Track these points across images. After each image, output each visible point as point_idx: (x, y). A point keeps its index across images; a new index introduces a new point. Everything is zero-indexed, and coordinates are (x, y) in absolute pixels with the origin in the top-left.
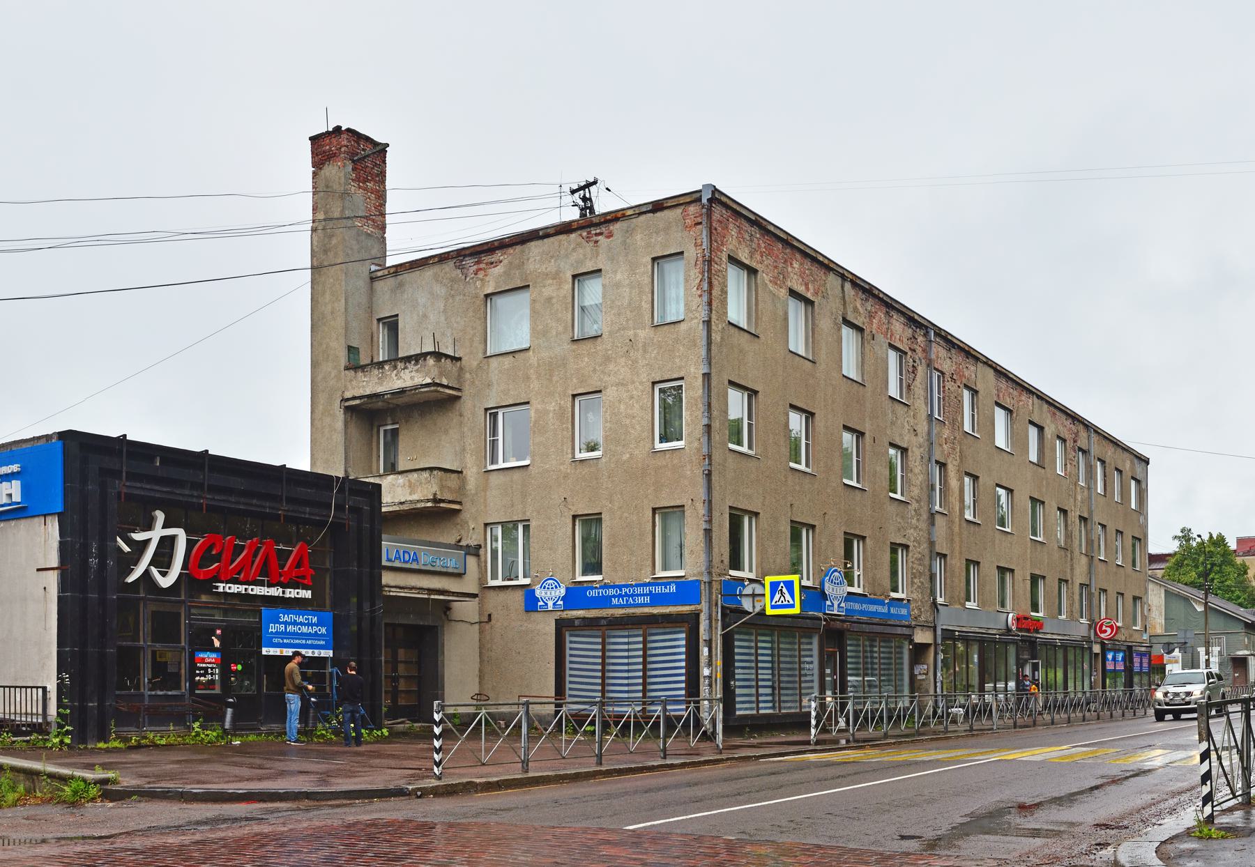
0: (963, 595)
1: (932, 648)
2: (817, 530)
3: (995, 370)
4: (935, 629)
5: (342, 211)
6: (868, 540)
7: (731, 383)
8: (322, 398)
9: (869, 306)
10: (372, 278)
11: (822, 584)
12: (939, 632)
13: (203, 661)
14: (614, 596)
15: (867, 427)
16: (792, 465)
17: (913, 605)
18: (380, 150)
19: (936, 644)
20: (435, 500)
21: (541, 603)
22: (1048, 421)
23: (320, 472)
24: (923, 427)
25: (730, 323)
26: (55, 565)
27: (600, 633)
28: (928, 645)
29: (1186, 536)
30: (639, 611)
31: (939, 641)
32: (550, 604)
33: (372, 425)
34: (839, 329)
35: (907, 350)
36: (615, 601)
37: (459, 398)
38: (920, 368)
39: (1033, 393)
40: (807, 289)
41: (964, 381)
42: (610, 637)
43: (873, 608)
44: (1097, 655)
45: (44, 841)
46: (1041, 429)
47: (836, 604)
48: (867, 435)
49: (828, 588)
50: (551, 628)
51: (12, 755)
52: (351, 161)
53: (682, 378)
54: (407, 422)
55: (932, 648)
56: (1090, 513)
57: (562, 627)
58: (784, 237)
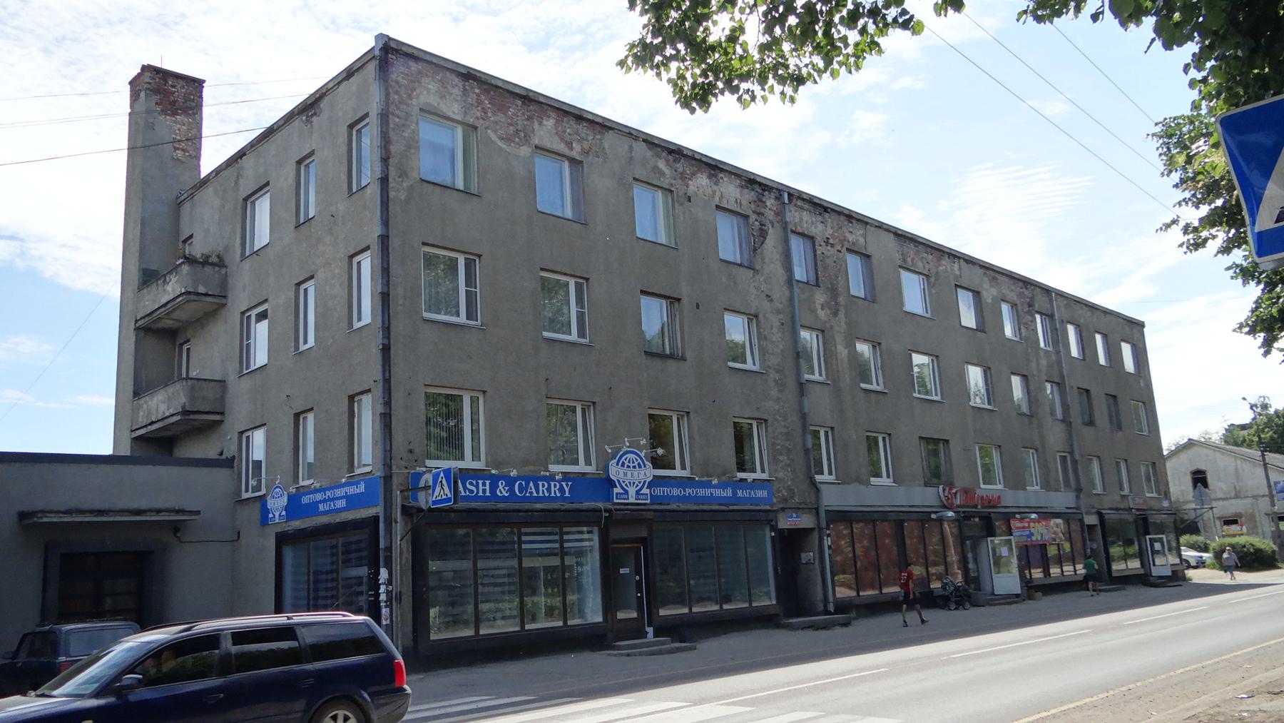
0: (221, 474)
1: (816, 534)
2: (598, 408)
3: (460, 75)
4: (817, 510)
5: (969, 538)
6: (692, 415)
7: (643, 292)
8: (1086, 313)
9: (680, 167)
10: (936, 441)
11: (606, 469)
12: (823, 514)
13: (484, 484)
14: (320, 502)
15: (684, 292)
16: (863, 385)
17: (776, 485)
18: (195, 85)
19: (820, 529)
20: (185, 412)
21: (617, 490)
22: (986, 286)
23: (111, 401)
24: (780, 293)
25: (422, 180)
26: (1169, 465)
27: (557, 530)
28: (812, 529)
29: (643, 55)
30: (339, 518)
31: (824, 524)
32: (632, 491)
33: (174, 344)
34: (629, 189)
35: (750, 212)
36: (321, 507)
37: (221, 422)
38: (771, 231)
39: (722, 170)
40: (571, 148)
41: (846, 245)
42: (568, 533)
43: (702, 492)
44: (1091, 527)
45: (1229, 522)
46: (977, 294)
47: (277, 515)
48: (685, 300)
49: (615, 472)
50: (271, 543)
51: (572, 184)
52: (166, 99)
53: (266, 301)
54: (203, 328)
55: (816, 534)
56: (1062, 377)
57: (283, 540)
58: (523, 93)
